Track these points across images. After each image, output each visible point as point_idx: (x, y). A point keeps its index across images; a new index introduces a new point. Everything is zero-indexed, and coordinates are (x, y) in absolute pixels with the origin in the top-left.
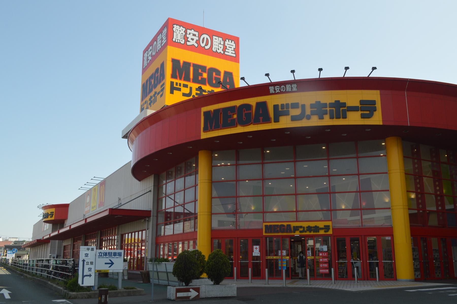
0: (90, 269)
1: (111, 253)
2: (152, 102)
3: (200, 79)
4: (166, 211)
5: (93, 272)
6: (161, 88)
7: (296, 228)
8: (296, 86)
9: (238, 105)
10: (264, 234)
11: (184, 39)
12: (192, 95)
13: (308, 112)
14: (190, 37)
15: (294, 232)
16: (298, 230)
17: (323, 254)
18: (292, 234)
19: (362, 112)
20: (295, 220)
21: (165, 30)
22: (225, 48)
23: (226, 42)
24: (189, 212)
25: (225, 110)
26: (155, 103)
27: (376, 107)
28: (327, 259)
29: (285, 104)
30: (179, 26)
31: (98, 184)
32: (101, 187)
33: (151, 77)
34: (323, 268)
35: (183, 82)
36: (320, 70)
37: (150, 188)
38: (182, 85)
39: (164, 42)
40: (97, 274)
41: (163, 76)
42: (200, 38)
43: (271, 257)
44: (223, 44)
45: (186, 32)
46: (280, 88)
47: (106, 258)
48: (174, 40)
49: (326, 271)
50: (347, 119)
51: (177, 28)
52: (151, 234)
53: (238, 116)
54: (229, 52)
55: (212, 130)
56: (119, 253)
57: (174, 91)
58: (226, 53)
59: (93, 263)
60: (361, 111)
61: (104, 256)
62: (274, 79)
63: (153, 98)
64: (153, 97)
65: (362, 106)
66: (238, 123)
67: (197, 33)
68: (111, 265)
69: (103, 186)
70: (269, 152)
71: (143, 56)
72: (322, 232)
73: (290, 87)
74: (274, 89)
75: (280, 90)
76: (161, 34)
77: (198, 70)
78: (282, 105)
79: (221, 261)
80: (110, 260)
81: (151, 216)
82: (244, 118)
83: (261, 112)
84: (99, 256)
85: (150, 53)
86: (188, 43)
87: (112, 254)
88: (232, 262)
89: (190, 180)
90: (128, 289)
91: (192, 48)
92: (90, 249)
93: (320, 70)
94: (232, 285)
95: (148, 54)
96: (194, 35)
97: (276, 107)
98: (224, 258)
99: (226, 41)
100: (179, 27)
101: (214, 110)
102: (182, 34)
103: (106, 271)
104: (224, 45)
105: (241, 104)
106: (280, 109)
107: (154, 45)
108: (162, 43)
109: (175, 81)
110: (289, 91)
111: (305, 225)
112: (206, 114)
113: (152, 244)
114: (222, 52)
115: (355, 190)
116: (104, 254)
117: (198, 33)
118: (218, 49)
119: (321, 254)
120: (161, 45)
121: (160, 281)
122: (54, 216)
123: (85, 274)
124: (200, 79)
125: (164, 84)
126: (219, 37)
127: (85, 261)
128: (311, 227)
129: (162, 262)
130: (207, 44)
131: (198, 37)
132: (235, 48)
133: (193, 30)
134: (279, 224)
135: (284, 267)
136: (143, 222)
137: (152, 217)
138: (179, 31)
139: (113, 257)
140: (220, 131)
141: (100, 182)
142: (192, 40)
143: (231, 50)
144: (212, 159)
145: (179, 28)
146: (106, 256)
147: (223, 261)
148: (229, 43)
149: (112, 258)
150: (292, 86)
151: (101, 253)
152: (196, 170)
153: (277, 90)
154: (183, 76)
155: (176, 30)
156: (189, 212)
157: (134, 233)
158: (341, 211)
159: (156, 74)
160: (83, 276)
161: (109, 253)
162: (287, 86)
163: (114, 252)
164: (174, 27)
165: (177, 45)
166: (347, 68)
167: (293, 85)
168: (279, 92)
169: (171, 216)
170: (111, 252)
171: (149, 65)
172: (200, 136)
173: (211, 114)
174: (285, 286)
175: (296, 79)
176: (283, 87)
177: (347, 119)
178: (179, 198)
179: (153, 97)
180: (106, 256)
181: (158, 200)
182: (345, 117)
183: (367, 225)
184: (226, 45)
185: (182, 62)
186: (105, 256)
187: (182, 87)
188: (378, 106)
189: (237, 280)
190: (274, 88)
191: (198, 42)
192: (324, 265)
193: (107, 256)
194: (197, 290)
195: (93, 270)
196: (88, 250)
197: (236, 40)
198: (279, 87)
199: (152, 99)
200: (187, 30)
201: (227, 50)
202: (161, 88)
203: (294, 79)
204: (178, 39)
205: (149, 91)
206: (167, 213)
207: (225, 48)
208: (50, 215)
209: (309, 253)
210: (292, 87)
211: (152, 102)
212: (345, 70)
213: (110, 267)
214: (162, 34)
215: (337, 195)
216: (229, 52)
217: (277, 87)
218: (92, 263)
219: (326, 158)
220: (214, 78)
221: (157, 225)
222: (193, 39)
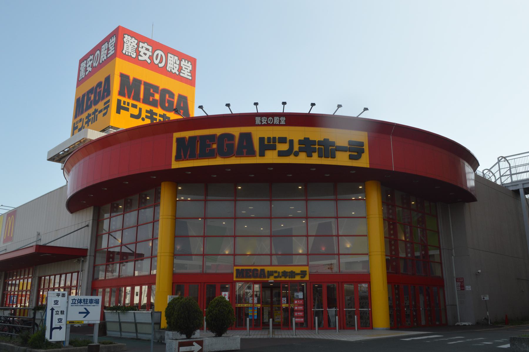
0: (60, 320)
1: (87, 300)
2: (90, 121)
3: (151, 100)
4: (109, 250)
5: (64, 324)
6: (104, 105)
7: (271, 273)
8: (285, 119)
9: (218, 134)
11: (135, 52)
13: (296, 148)
14: (143, 51)
15: (268, 278)
16: (272, 275)
17: (299, 301)
18: (266, 279)
19: (351, 153)
20: (269, 264)
21: (114, 39)
22: (180, 69)
24: (132, 252)
25: (203, 138)
26: (94, 122)
27: (364, 149)
28: (302, 307)
29: (272, 137)
30: (131, 37)
31: (4, 214)
32: (9, 218)
33: (91, 91)
34: (298, 317)
35: (131, 102)
36: (284, 103)
37: (88, 222)
38: (130, 105)
39: (111, 52)
40: (69, 326)
41: (108, 91)
43: (242, 305)
44: (178, 64)
45: (138, 44)
47: (81, 306)
48: (124, 52)
49: (301, 319)
50: (335, 159)
51: (128, 38)
52: (87, 276)
53: (218, 146)
54: (184, 74)
55: (186, 159)
56: (96, 299)
57: (121, 110)
58: (181, 74)
59: (63, 313)
60: (350, 151)
61: (78, 304)
62: (262, 109)
63: (93, 116)
64: (92, 115)
65: (350, 146)
66: (217, 153)
67: (150, 48)
68: (86, 314)
69: (13, 216)
70: (301, 187)
71: (80, 66)
73: (279, 119)
74: (260, 120)
75: (267, 122)
76: (106, 44)
77: (150, 90)
78: (269, 138)
79: (227, 309)
80: (85, 309)
82: (226, 149)
83: (245, 144)
84: (72, 303)
85: (90, 63)
86: (140, 58)
87: (88, 301)
89: (147, 213)
90: (107, 344)
91: (143, 64)
92: (61, 295)
93: (284, 103)
94: (234, 337)
95: (86, 64)
96: (147, 49)
97: (262, 140)
98: (229, 307)
99: (182, 61)
101: (190, 137)
102: (134, 46)
103: (80, 322)
104: (180, 64)
105: (222, 133)
106: (266, 143)
107: (96, 54)
108: (108, 54)
109: (123, 99)
110: (277, 123)
111: (281, 269)
112: (179, 140)
113: (87, 289)
114: (177, 73)
115: (314, 234)
116: (78, 301)
117: (151, 48)
118: (173, 69)
119: (296, 302)
120: (107, 56)
121: (123, 334)
123: (53, 326)
124: (151, 100)
125: (108, 101)
126: (174, 55)
127: (54, 310)
128: (287, 272)
129: (129, 311)
130: (161, 62)
132: (191, 70)
133: (146, 44)
134: (252, 268)
135: (255, 315)
136: (75, 262)
137: (88, 257)
138: (130, 42)
139: (89, 304)
140: (195, 161)
141: (8, 212)
142: (144, 54)
143: (187, 72)
144: (176, 193)
145: (131, 39)
146: (80, 303)
147: (228, 310)
148: (185, 64)
149: (88, 306)
150: (281, 118)
151: (74, 299)
152: (155, 204)
153: (264, 121)
154: (132, 94)
155: (127, 41)
156: (132, 252)
157: (65, 275)
158: (298, 256)
159: (98, 89)
160: (52, 329)
161: (84, 300)
162: (275, 119)
163: (90, 299)
165: (128, 58)
166: (313, 105)
167: (281, 118)
168: (266, 123)
169: (114, 255)
170: (87, 299)
171: (87, 77)
172: (171, 165)
173: (186, 141)
174: (272, 337)
175: (259, 112)
177: (335, 159)
178: (129, 236)
179: (92, 115)
180: (80, 303)
181: (97, 237)
182: (333, 157)
183: (344, 270)
184: (182, 65)
185: (131, 79)
186: (79, 304)
187: (130, 107)
188: (366, 148)
189: (340, 331)
191: (151, 57)
192: (300, 313)
193: (82, 304)
194: (200, 343)
195: (64, 321)
196: (58, 296)
198: (266, 118)
199: (90, 118)
200: (139, 43)
201: (182, 71)
202: (104, 105)
203: (257, 112)
204: (128, 52)
205: (86, 107)
206: (109, 253)
207: (180, 69)
209: (284, 300)
210: (281, 119)
211: (90, 121)
212: (311, 106)
213: (85, 317)
214: (108, 43)
215: (293, 238)
216: (184, 74)
218: (62, 312)
219: (233, 198)
220: (166, 100)
221: (94, 266)
222: (145, 54)
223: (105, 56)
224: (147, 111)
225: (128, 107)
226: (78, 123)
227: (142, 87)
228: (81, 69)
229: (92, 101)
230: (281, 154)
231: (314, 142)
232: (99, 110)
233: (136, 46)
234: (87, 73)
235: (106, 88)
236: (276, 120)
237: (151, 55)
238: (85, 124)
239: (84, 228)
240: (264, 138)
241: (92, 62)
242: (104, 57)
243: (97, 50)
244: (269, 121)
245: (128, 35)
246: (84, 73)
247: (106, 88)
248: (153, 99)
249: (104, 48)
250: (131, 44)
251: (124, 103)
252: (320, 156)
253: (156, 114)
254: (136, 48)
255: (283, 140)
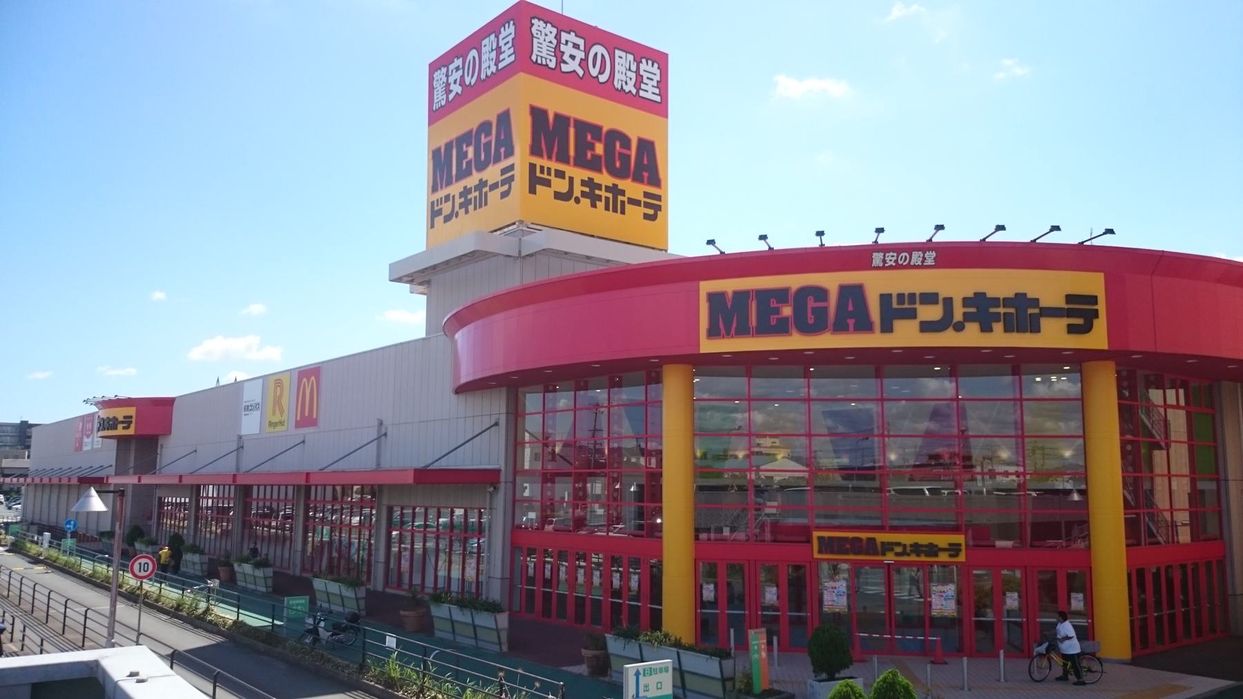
2: (470, 204)
10: (816, 555)
12: (574, 196)
14: (568, 50)
15: (884, 554)
16: (892, 550)
22: (639, 80)
23: (641, 64)
30: (545, 22)
32: (305, 380)
33: (465, 139)
35: (555, 165)
38: (553, 172)
42: (589, 52)
45: (558, 37)
46: (897, 259)
48: (534, 58)
54: (647, 91)
57: (537, 186)
58: (642, 93)
64: (475, 191)
67: (581, 42)
69: (313, 378)
72: (943, 557)
73: (922, 255)
75: (896, 261)
76: (493, 36)
81: (500, 483)
83: (851, 308)
85: (458, 75)
88: (743, 612)
95: (447, 76)
96: (576, 46)
97: (885, 299)
100: (544, 25)
101: (736, 293)
102: (550, 42)
106: (895, 305)
107: (470, 57)
109: (539, 162)
110: (917, 264)
112: (712, 297)
114: (634, 91)
118: (626, 83)
120: (496, 65)
122: (133, 426)
130: (601, 72)
131: (585, 51)
137: (502, 486)
138: (543, 34)
150: (926, 255)
153: (891, 260)
159: (483, 136)
164: (533, 24)
165: (540, 70)
168: (894, 264)
172: (698, 345)
176: (903, 258)
182: (1036, 329)
184: (642, 73)
187: (552, 178)
190: (884, 256)
191: (583, 64)
197: (660, 59)
198: (895, 254)
201: (643, 86)
204: (542, 57)
207: (639, 80)
208: (122, 422)
210: (926, 256)
214: (497, 37)
216: (647, 91)
217: (891, 254)
223: (492, 64)
224: (583, 183)
225: (548, 177)
226: (441, 204)
227: (572, 131)
228: (435, 86)
229: (471, 161)
230: (926, 327)
231: (995, 302)
232: (489, 183)
233: (555, 42)
234: (451, 96)
235: (502, 137)
236: (916, 258)
237: (583, 57)
238: (460, 208)
239: (488, 431)
240: (890, 295)
241: (460, 72)
242: (489, 67)
243: (471, 49)
244: (901, 260)
245: (539, 20)
246: (445, 97)
247: (502, 137)
248: (593, 156)
249: (487, 45)
250: (546, 37)
251: (542, 168)
252: (1007, 329)
253: (599, 187)
254: (556, 46)
255: (929, 298)
